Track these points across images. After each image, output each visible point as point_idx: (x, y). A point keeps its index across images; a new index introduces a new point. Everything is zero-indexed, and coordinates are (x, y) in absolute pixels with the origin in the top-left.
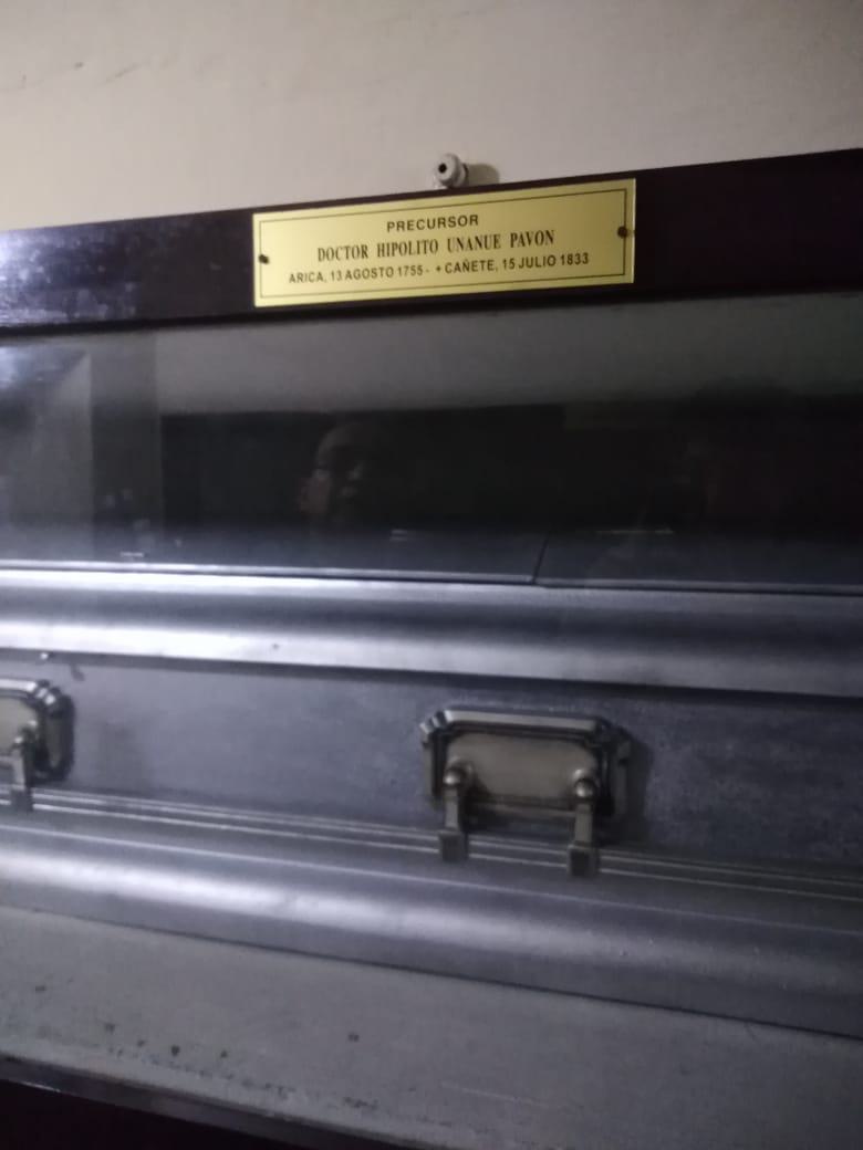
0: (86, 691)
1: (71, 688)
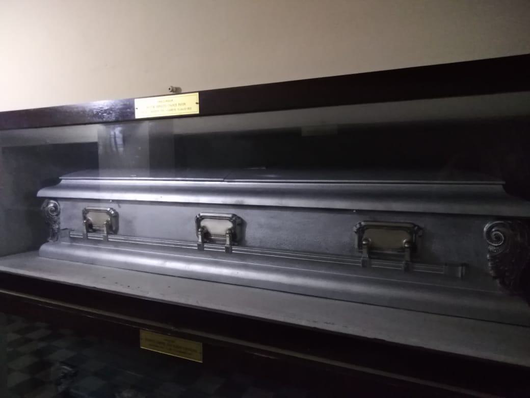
0: (123, 210)
1: (118, 210)
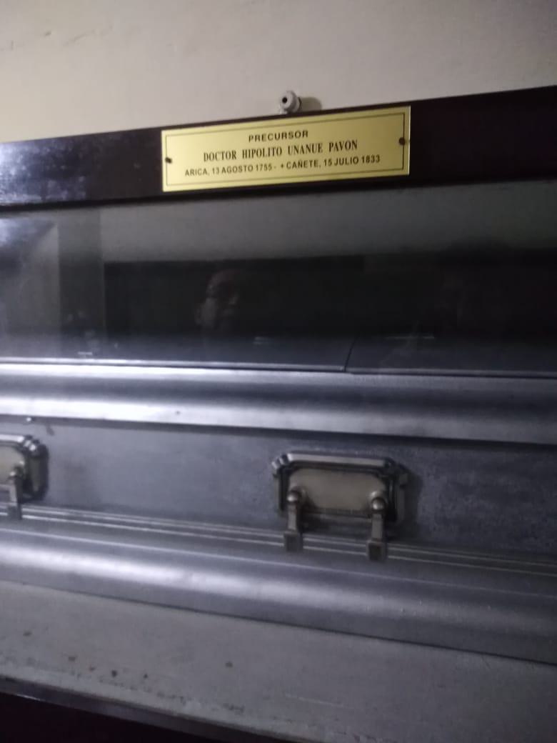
0: (56, 442)
1: (46, 440)
